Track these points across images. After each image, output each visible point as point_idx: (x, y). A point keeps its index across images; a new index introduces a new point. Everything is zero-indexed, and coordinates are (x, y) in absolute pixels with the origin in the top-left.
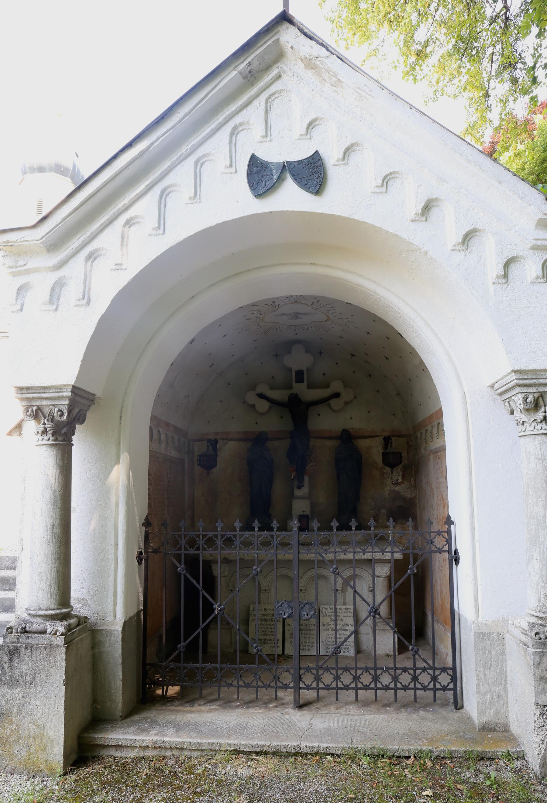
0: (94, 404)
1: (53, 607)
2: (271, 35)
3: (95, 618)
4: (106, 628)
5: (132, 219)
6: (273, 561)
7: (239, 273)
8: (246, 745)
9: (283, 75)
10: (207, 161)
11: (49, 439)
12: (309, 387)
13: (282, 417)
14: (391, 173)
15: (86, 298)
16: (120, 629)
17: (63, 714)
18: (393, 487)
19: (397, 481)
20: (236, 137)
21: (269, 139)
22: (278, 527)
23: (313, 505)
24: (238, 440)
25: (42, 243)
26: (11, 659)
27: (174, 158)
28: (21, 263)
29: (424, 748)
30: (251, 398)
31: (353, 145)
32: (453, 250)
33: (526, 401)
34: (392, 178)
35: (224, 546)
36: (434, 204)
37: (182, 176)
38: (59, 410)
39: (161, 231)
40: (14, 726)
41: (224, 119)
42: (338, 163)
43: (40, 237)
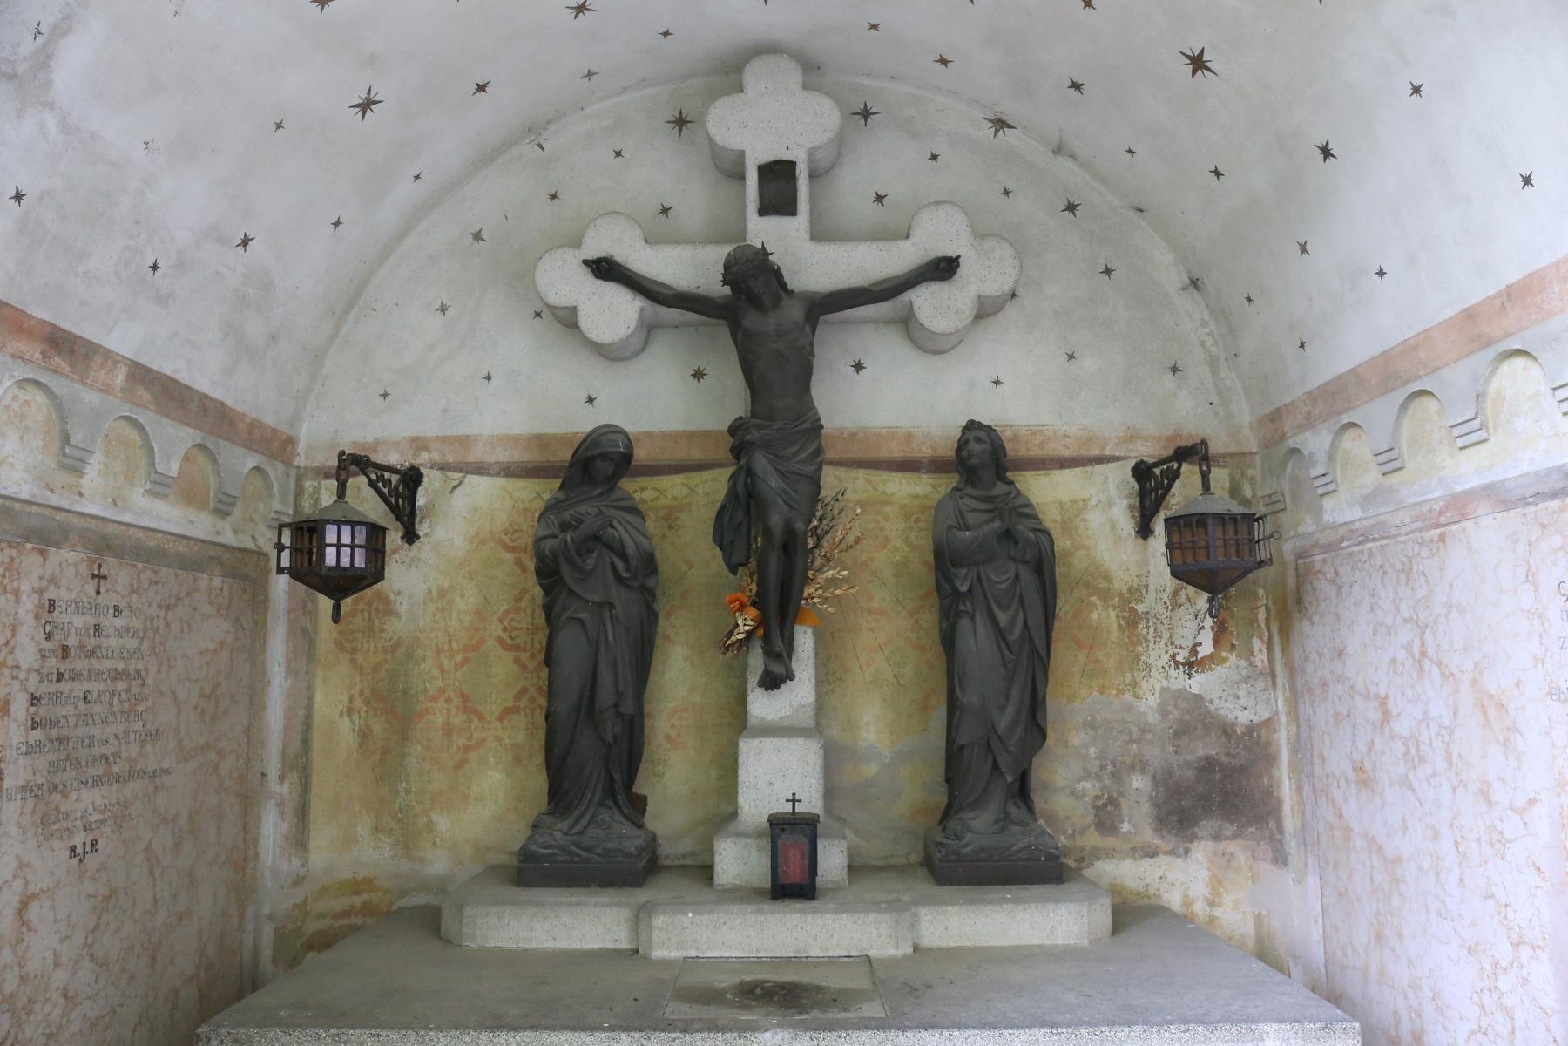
12: (819, 234)
13: (698, 375)
18: (1178, 680)
19: (1194, 651)
23: (833, 760)
24: (508, 471)
30: (565, 281)
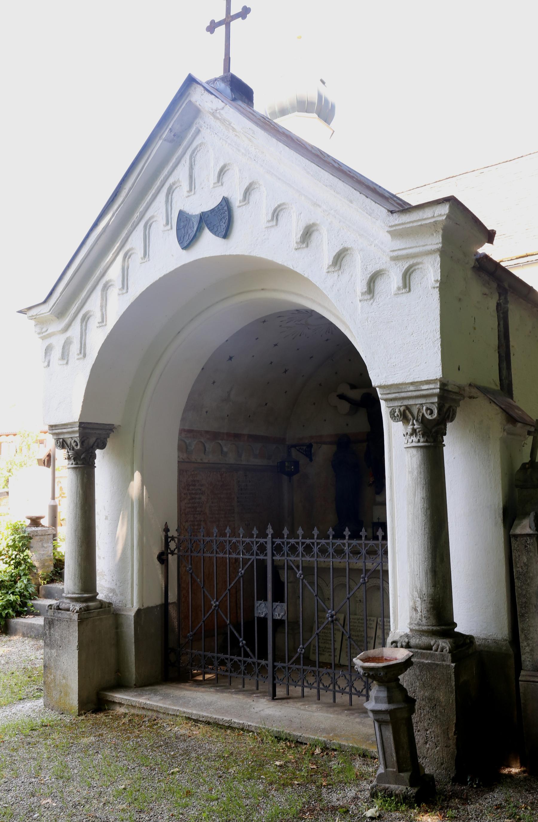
0: (113, 432)
1: (77, 592)
2: (184, 99)
3: (121, 605)
4: (122, 613)
5: (107, 283)
6: (379, 571)
7: (208, 307)
8: (196, 714)
9: (200, 129)
10: (153, 222)
11: (72, 464)
14: (279, 206)
15: (83, 352)
16: (133, 614)
17: (77, 671)
20: (172, 195)
21: (193, 193)
22: (349, 536)
25: (51, 314)
26: (50, 628)
27: (129, 226)
28: (44, 330)
29: (320, 738)
31: (251, 185)
32: (328, 272)
33: (394, 414)
34: (282, 210)
35: (290, 553)
36: (313, 229)
37: (136, 241)
38: (75, 441)
39: (125, 291)
40: (52, 676)
41: (160, 183)
42: (241, 204)
43: (48, 310)
